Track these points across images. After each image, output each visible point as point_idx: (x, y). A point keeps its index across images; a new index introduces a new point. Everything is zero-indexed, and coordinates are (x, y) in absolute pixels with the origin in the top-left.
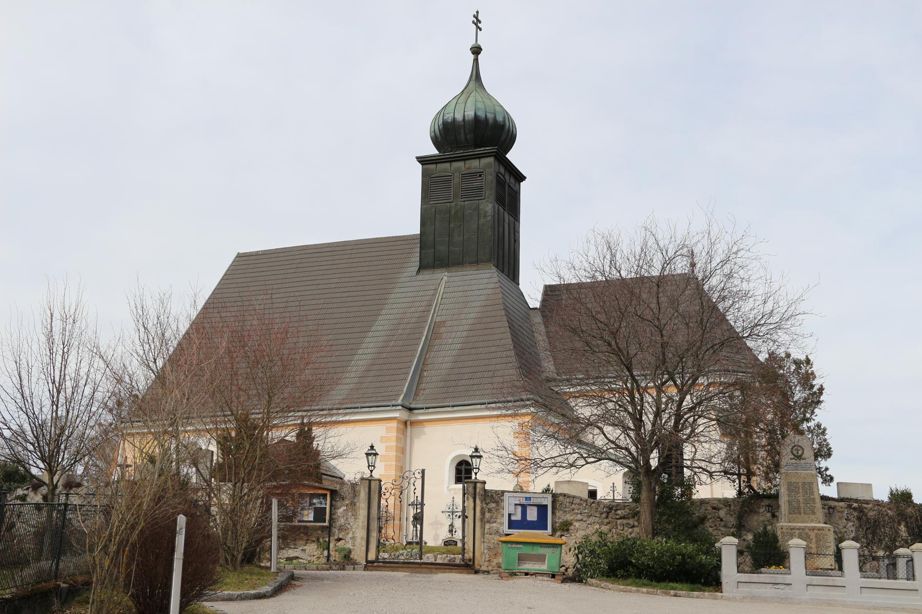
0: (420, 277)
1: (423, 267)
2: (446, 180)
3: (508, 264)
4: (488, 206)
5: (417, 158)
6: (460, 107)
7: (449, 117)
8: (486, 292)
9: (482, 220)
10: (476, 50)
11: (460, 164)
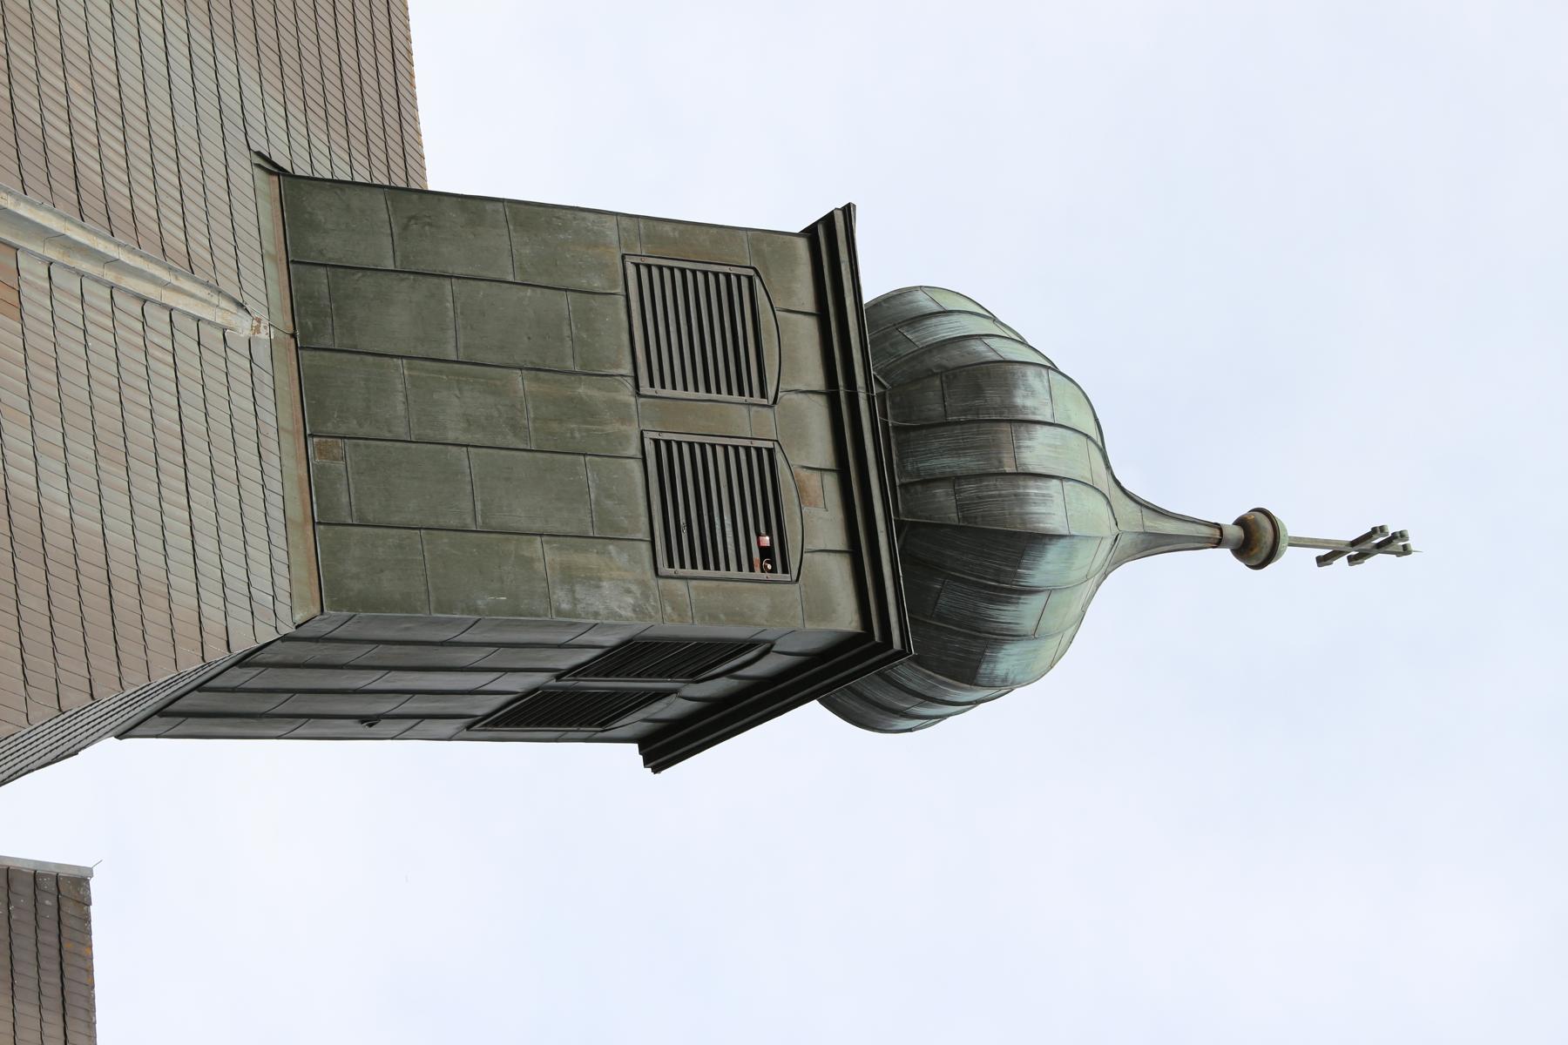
0: (244, 172)
1: (294, 191)
2: (739, 367)
4: (624, 595)
5: (848, 210)
6: (1081, 461)
7: (1032, 397)
8: (183, 581)
9: (547, 556)
11: (818, 448)
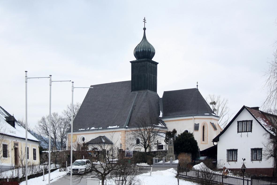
0: (132, 93)
3: (155, 89)
10: (145, 29)
